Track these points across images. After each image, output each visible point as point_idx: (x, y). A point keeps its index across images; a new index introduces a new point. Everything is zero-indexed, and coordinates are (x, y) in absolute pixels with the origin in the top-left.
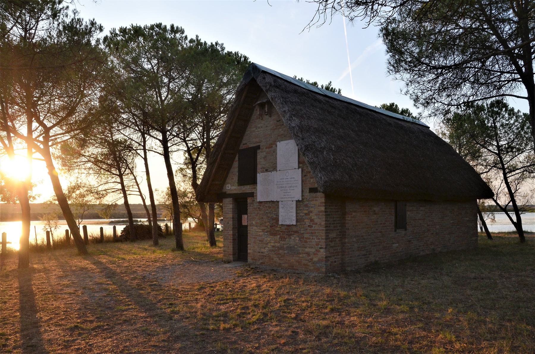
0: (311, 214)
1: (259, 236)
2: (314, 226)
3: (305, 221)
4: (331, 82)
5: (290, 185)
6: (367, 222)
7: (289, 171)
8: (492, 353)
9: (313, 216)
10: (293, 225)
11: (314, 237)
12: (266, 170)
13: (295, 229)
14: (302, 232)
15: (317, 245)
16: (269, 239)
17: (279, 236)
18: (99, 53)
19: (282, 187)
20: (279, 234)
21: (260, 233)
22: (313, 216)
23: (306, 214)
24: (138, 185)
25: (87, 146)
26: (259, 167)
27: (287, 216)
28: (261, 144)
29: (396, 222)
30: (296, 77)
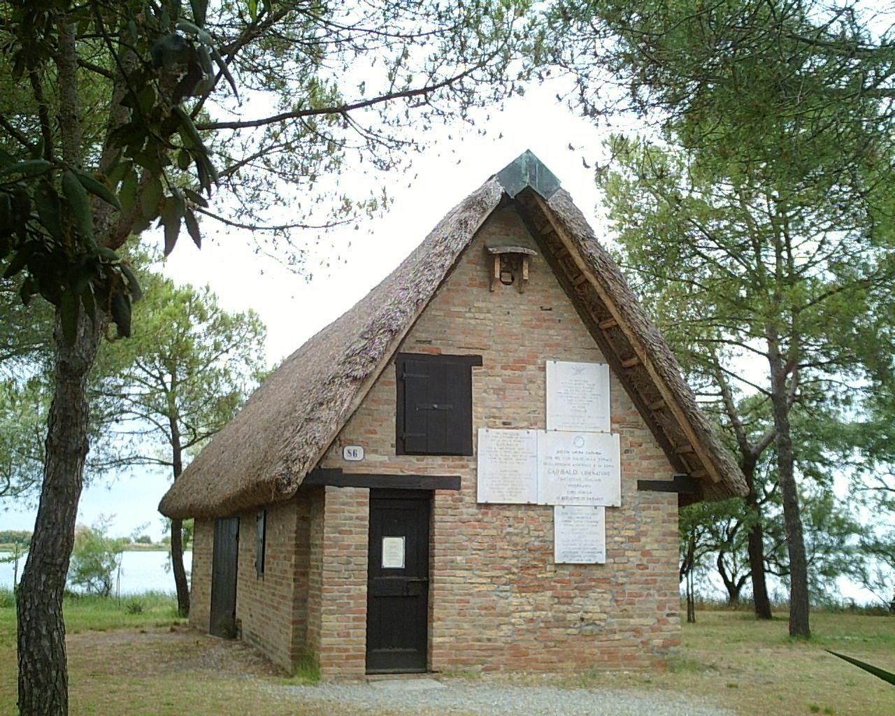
0: (643, 539)
1: (479, 594)
2: (651, 566)
3: (627, 553)
4: (364, 83)
5: (589, 469)
6: (616, 426)
8: (886, 526)
11: (652, 592)
12: (504, 424)
15: (660, 608)
16: (515, 601)
18: (69, 54)
19: (563, 472)
20: (553, 588)
23: (631, 539)
24: (237, 225)
25: (313, 610)
28: (486, 356)
29: (399, 438)
30: (768, 378)
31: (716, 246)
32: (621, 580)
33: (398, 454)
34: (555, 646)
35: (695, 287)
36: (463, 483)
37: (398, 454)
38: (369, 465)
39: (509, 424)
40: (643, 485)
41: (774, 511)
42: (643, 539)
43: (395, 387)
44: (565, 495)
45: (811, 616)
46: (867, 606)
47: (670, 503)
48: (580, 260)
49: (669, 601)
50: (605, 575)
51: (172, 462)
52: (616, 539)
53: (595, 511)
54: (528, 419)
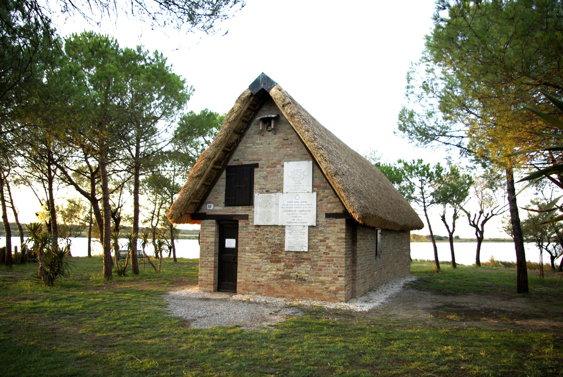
0: (327, 241)
5: (301, 209)
7: (300, 195)
9: (330, 242)
10: (304, 252)
13: (305, 256)
14: (315, 259)
17: (283, 264)
19: (290, 211)
20: (284, 262)
21: (256, 261)
22: (330, 242)
23: (321, 241)
26: (256, 187)
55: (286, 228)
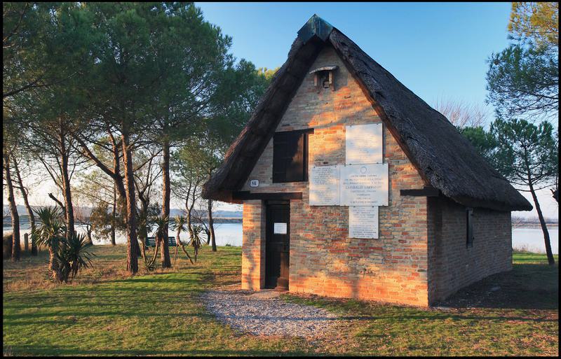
0: (403, 225)
3: (393, 233)
11: (408, 256)
12: (324, 163)
27: (363, 224)
31: (111, 166)
32: (388, 249)
33: (273, 182)
34: (121, 293)
35: (72, 167)
36: (303, 195)
37: (273, 182)
38: (261, 188)
39: (327, 163)
40: (404, 193)
41: (13, 170)
42: (403, 225)
43: (272, 149)
44: (355, 200)
45: (259, 278)
46: (208, 23)
47: (421, 203)
48: (351, 110)
49: (419, 262)
50: (380, 246)
51: (426, 269)
52: (386, 225)
53: (373, 209)
54: (337, 159)
55: (350, 210)
